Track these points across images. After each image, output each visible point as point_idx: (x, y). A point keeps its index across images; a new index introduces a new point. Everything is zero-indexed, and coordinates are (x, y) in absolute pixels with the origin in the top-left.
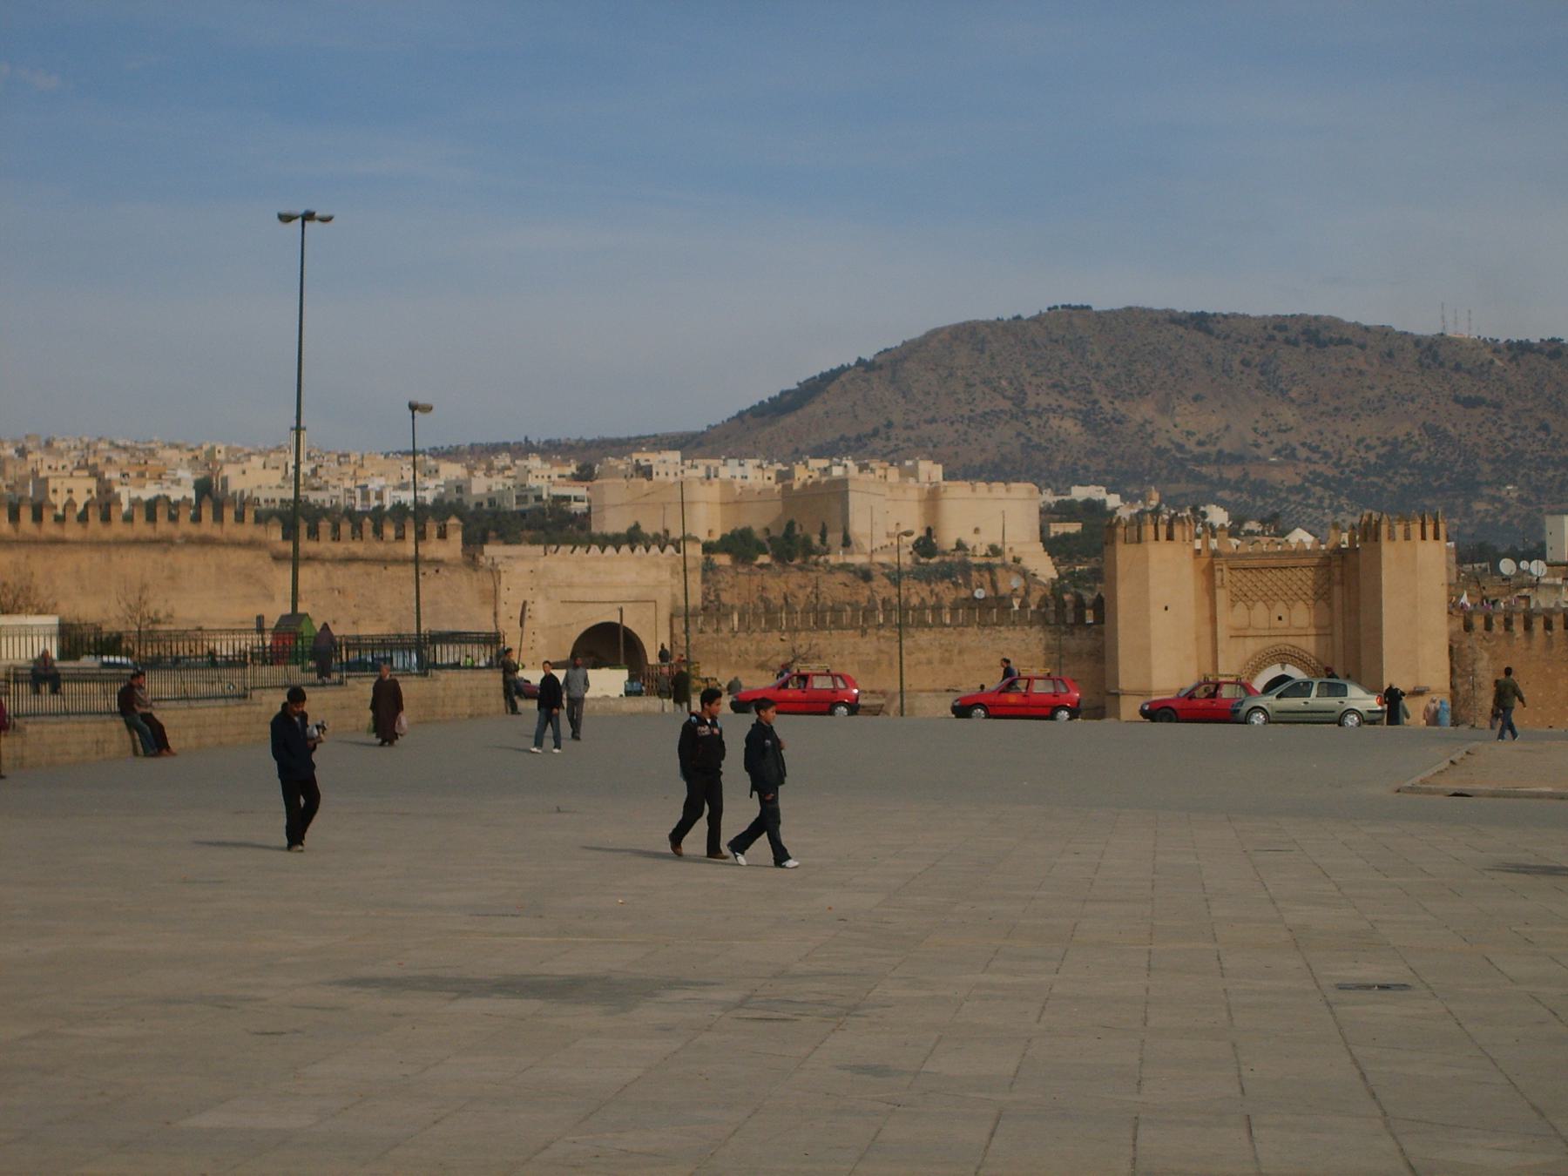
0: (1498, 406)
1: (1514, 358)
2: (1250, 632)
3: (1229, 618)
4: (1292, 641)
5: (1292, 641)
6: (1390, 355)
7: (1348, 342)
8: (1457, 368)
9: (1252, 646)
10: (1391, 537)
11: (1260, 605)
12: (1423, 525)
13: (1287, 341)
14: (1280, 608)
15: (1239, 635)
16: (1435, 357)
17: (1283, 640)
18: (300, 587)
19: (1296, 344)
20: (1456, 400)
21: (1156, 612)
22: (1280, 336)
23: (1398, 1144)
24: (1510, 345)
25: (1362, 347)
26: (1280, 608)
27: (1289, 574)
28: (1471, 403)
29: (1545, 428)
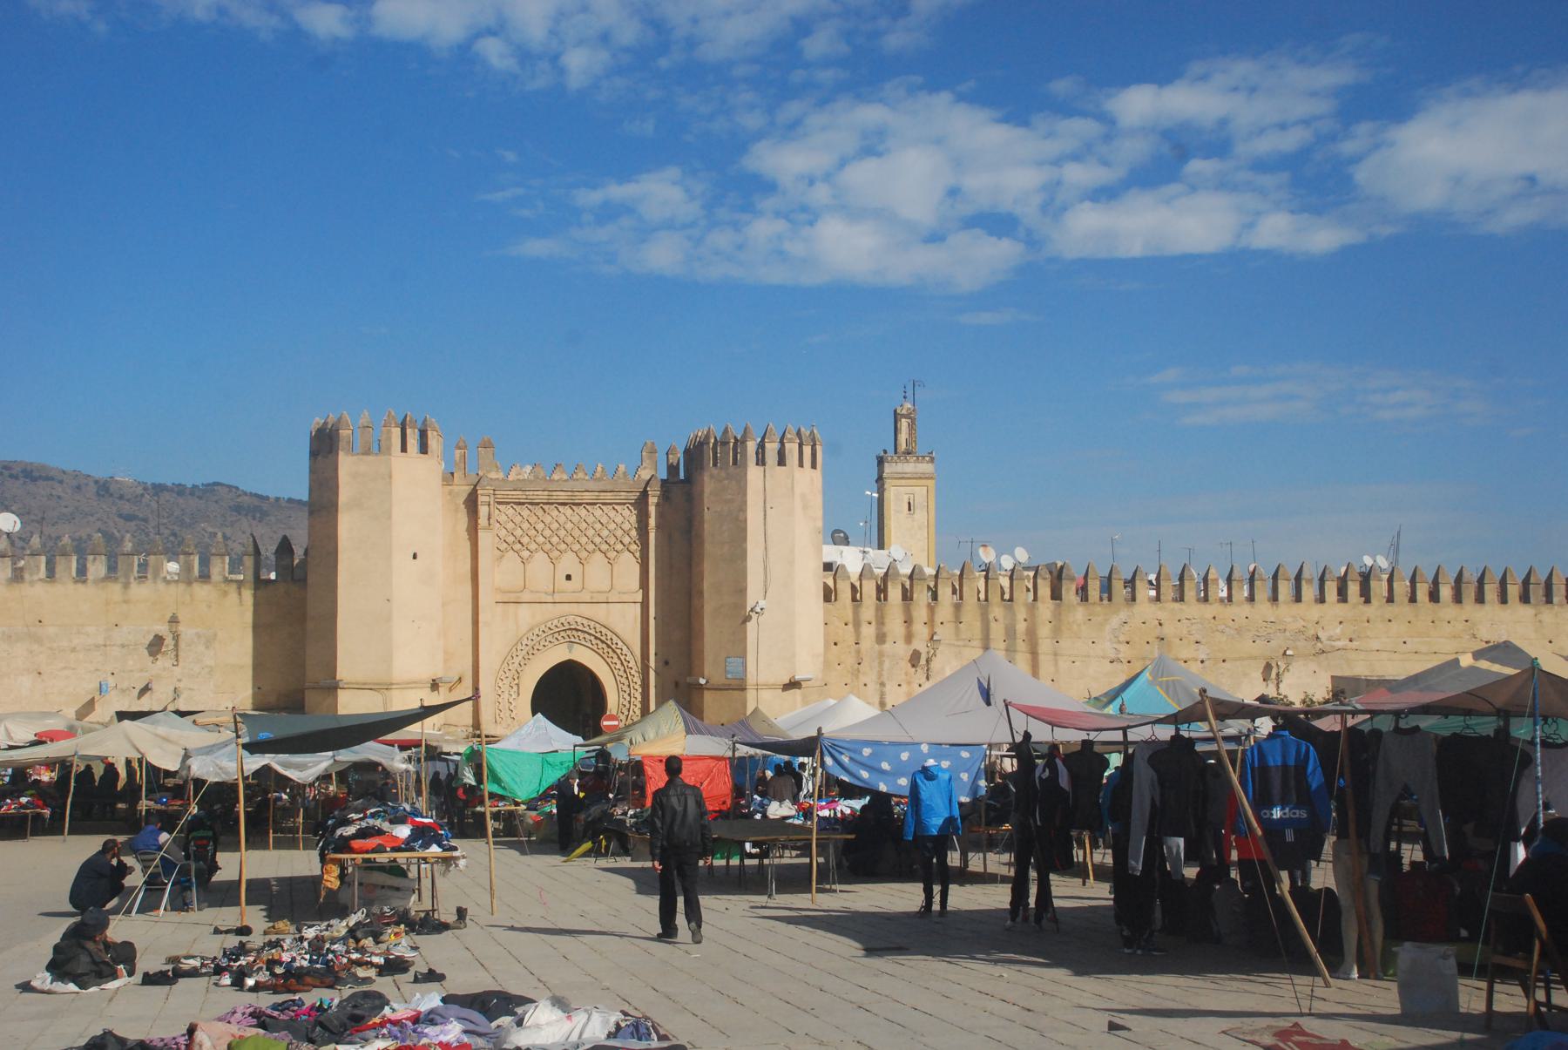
0: (145, 520)
1: (156, 494)
2: (526, 597)
3: (498, 573)
4: (586, 610)
5: (586, 610)
6: (79, 487)
7: (52, 479)
8: (121, 497)
9: (526, 616)
10: (761, 461)
11: (540, 556)
12: (801, 446)
13: (11, 476)
14: (568, 563)
15: (511, 600)
16: (107, 490)
17: (574, 608)
18: (1211, 1019)
19: (17, 478)
20: (120, 516)
21: (401, 560)
22: (6, 473)
23: (193, 973)
24: (154, 486)
25: (61, 482)
26: (568, 563)
27: (583, 512)
28: (129, 518)
29: (174, 535)
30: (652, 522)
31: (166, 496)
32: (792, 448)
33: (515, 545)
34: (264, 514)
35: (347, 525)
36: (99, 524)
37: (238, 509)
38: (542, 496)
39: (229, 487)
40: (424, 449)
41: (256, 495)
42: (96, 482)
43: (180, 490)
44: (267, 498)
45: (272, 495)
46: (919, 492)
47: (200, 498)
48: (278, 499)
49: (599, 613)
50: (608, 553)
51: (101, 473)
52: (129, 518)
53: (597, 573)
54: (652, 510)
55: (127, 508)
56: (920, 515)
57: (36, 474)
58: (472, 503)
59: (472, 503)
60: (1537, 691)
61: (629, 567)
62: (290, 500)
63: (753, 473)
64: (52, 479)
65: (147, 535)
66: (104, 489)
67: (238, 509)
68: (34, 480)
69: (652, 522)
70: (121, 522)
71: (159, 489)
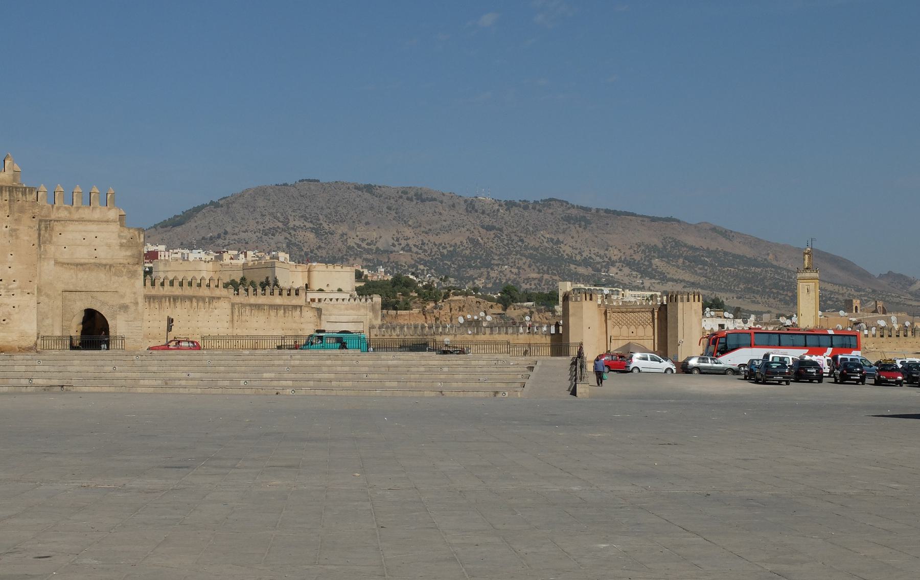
0: (501, 230)
6: (454, 206)
7: (435, 200)
8: (483, 213)
10: (682, 300)
13: (408, 199)
14: (633, 328)
20: (483, 227)
22: (405, 196)
25: (441, 202)
26: (633, 328)
28: (489, 228)
29: (522, 241)
30: (656, 316)
31: (515, 210)
32: (691, 297)
33: (617, 324)
34: (588, 222)
35: (572, 320)
36: (468, 234)
37: (568, 219)
38: (624, 310)
39: (561, 202)
40: (591, 299)
41: (582, 208)
42: (466, 201)
43: (525, 205)
44: (590, 209)
45: (594, 207)
46: (812, 285)
47: (540, 211)
48: (598, 210)
49: (641, 342)
50: (644, 326)
51: (468, 195)
52: (489, 228)
53: (641, 331)
54: (656, 314)
55: (487, 220)
56: (812, 294)
57: (424, 196)
58: (606, 313)
59: (606, 313)
60: (916, 365)
61: (649, 330)
62: (607, 211)
63: (680, 304)
64: (435, 200)
65: (502, 241)
66: (471, 206)
67: (568, 219)
68: (423, 201)
69: (656, 316)
70: (483, 231)
71: (510, 205)
